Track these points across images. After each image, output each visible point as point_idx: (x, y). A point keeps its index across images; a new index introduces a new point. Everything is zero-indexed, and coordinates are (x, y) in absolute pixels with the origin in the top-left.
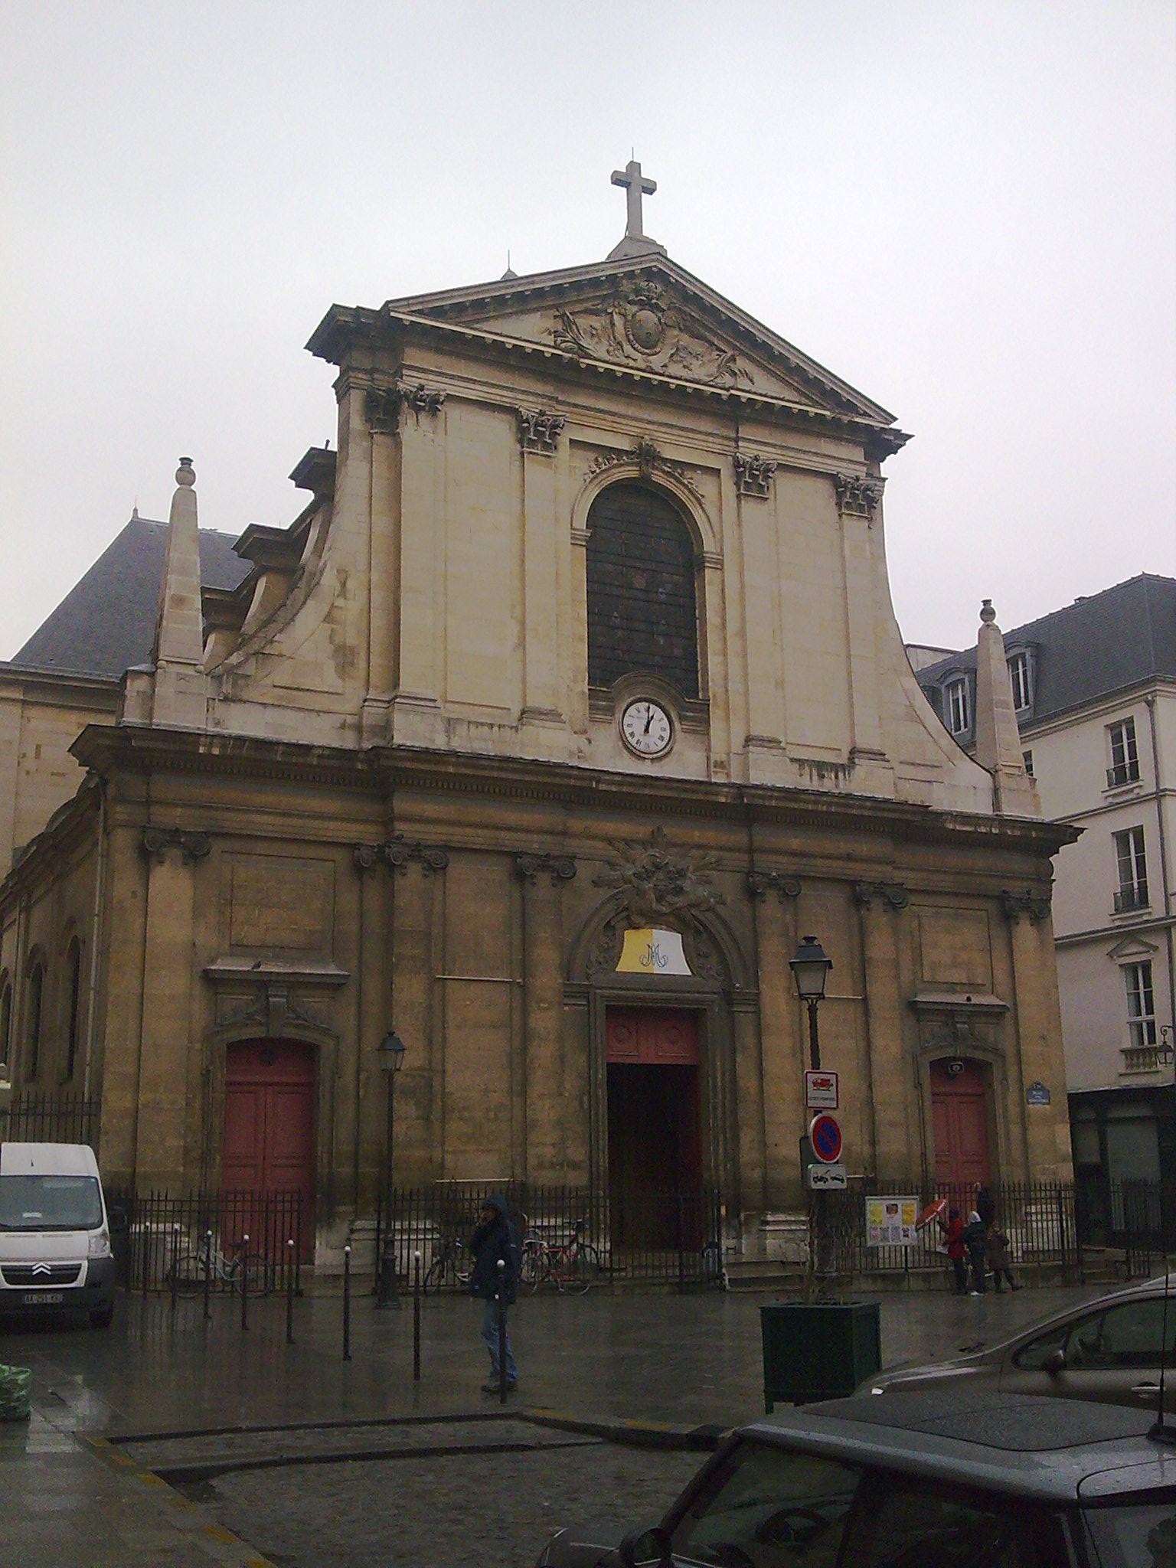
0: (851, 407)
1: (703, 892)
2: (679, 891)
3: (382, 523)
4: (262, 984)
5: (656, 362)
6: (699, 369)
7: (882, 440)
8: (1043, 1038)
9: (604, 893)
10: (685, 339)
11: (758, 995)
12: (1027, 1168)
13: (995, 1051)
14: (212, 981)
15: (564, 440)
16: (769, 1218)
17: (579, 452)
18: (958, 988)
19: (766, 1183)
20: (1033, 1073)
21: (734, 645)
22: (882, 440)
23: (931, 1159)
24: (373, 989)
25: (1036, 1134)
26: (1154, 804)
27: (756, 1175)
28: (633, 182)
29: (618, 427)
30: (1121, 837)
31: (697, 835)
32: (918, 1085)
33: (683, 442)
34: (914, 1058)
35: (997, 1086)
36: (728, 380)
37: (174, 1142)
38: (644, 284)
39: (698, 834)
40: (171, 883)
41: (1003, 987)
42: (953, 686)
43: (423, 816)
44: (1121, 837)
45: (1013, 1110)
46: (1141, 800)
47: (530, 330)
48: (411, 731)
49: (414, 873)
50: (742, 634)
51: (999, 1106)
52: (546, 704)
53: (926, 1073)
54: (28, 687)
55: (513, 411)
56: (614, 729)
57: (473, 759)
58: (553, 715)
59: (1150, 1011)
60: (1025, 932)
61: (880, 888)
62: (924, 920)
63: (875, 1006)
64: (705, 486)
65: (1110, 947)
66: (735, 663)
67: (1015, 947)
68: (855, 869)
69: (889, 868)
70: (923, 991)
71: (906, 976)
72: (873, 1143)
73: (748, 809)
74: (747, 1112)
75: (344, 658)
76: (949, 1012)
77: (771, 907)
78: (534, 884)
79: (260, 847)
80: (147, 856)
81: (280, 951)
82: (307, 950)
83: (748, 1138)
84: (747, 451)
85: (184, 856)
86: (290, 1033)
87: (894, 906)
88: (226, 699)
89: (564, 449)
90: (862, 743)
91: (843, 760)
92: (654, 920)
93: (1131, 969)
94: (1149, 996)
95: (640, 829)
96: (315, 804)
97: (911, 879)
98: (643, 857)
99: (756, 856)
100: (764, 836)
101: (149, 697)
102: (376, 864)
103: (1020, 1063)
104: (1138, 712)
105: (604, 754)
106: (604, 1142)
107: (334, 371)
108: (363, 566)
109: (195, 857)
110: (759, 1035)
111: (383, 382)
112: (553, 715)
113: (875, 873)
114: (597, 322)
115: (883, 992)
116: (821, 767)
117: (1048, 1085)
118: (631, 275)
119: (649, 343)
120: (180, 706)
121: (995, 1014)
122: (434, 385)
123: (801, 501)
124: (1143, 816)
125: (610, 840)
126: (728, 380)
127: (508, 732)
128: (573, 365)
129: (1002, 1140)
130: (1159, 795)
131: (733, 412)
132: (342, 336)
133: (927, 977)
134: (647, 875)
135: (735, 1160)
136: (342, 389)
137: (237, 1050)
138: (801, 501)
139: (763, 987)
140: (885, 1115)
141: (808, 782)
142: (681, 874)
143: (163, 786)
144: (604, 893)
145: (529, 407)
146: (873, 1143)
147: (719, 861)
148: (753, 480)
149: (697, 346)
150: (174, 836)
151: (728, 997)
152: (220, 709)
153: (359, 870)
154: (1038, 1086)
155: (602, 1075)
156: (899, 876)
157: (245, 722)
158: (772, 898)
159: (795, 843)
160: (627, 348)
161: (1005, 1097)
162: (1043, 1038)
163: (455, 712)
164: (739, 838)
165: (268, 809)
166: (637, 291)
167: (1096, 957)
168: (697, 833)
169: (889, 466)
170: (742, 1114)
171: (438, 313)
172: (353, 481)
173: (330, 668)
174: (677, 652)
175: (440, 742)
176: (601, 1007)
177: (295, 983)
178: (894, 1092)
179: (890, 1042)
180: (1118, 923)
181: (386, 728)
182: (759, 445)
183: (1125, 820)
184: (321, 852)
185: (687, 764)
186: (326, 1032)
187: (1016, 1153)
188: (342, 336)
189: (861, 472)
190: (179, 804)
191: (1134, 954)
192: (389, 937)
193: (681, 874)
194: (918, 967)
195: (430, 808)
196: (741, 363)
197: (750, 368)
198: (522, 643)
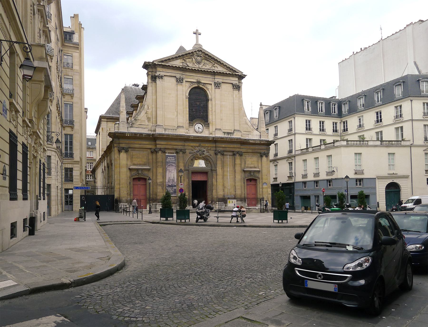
0: (235, 71)
1: (207, 154)
2: (204, 154)
3: (154, 97)
4: (137, 170)
5: (200, 66)
6: (208, 66)
7: (241, 77)
9: (191, 155)
10: (206, 61)
13: (258, 177)
14: (130, 170)
15: (184, 81)
17: (187, 83)
20: (264, 181)
21: (214, 113)
22: (241, 77)
24: (154, 170)
25: (265, 190)
28: (197, 33)
29: (194, 78)
30: (290, 141)
31: (207, 145)
32: (244, 183)
33: (205, 79)
36: (213, 68)
37: (125, 192)
38: (198, 53)
39: (207, 145)
40: (123, 155)
41: (260, 167)
42: (276, 109)
43: (161, 144)
44: (290, 141)
45: (261, 187)
47: (178, 63)
48: (159, 131)
49: (160, 153)
50: (215, 112)
51: (258, 186)
52: (181, 125)
54: (107, 119)
55: (175, 77)
56: (193, 128)
57: (168, 135)
58: (183, 127)
60: (264, 158)
61: (238, 152)
63: (236, 171)
64: (209, 87)
66: (214, 116)
71: (243, 166)
73: (215, 141)
74: (214, 187)
75: (149, 119)
76: (250, 172)
77: (219, 156)
79: (137, 149)
80: (119, 151)
81: (140, 165)
82: (144, 165)
83: (214, 191)
84: (216, 80)
86: (142, 177)
87: (241, 155)
88: (131, 127)
89: (184, 83)
90: (236, 129)
91: (233, 132)
92: (199, 158)
93: (290, 163)
95: (197, 144)
96: (145, 143)
97: (243, 150)
98: (197, 149)
100: (219, 145)
101: (118, 127)
102: (154, 152)
104: (292, 119)
105: (192, 133)
106: (191, 192)
107: (146, 71)
108: (151, 104)
111: (154, 74)
112: (183, 127)
113: (237, 150)
114: (190, 60)
116: (228, 133)
118: (196, 51)
119: (199, 63)
120: (123, 128)
121: (259, 172)
122: (162, 74)
123: (226, 88)
124: (292, 137)
125: (192, 146)
126: (213, 68)
127: (174, 130)
128: (186, 68)
130: (295, 134)
131: (214, 74)
132: (146, 66)
134: (198, 152)
135: (212, 195)
136: (148, 74)
137: (134, 179)
138: (226, 88)
140: (237, 187)
141: (226, 136)
142: (204, 151)
143: (121, 141)
144: (191, 155)
145: (178, 76)
147: (210, 149)
148: (217, 85)
149: (208, 62)
150: (123, 148)
151: (212, 170)
152: (129, 128)
153: (152, 152)
155: (191, 182)
156: (241, 150)
157: (133, 130)
158: (219, 154)
159: (223, 146)
160: (195, 64)
163: (167, 127)
164: (214, 145)
165: (137, 144)
166: (197, 54)
167: (284, 161)
169: (243, 81)
170: (213, 188)
171: (162, 61)
172: (149, 89)
173: (146, 121)
174: (205, 115)
175: (164, 132)
176: (191, 172)
177: (142, 170)
178: (239, 184)
179: (239, 176)
181: (155, 131)
182: (219, 79)
183: (290, 138)
184: (146, 150)
185: (206, 134)
186: (147, 176)
187: (261, 193)
188: (146, 66)
189: (237, 82)
190: (124, 144)
192: (157, 162)
193: (204, 151)
195: (163, 143)
196: (216, 65)
197: (217, 65)
198: (177, 116)
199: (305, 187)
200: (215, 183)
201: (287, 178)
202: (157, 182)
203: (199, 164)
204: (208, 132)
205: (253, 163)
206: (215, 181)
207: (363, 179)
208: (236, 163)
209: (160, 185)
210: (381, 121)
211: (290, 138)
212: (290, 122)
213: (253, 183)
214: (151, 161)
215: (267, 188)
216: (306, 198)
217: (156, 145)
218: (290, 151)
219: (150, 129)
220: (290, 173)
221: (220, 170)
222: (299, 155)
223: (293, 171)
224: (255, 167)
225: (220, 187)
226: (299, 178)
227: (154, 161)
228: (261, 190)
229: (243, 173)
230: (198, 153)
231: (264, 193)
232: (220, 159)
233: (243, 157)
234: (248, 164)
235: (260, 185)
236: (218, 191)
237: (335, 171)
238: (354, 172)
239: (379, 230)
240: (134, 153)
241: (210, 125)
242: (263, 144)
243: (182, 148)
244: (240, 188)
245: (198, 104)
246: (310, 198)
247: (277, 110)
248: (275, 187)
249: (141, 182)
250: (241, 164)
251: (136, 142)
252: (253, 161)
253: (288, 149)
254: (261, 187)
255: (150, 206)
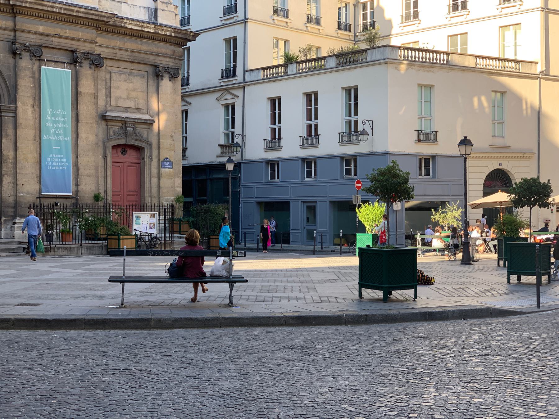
8: (172, 136)
11: (16, 108)
12: (159, 198)
16: (17, 221)
18: (129, 110)
19: (16, 204)
23: (110, 193)
26: (243, 25)
27: (11, 199)
30: (227, 41)
32: (105, 157)
34: (104, 143)
35: (147, 160)
44: (227, 41)
45: (154, 171)
46: (236, 23)
53: (109, 152)
59: (233, 127)
61: (87, 56)
62: (113, 74)
63: (81, 117)
65: (217, 95)
67: (79, 83)
68: (73, 45)
69: (94, 46)
70: (111, 111)
71: (101, 102)
72: (77, 185)
76: (125, 122)
77: (25, 62)
78: (21, 58)
85: (30, 56)
93: (226, 107)
94: (233, 120)
99: (18, 34)
103: (159, 148)
109: (97, 66)
110: (15, 128)
113: (86, 47)
115: (87, 110)
117: (172, 160)
124: (236, 31)
129: (147, 185)
133: (113, 103)
139: (19, 104)
146: (77, 185)
154: (167, 160)
156: (98, 50)
159: (41, 29)
161: (150, 164)
162: (172, 136)
168: (4, 22)
178: (91, 160)
179: (90, 134)
180: (222, 84)
183: (228, 33)
187: (154, 190)
191: (228, 99)
194: (108, 99)
199: (273, 177)
201: (219, 150)
205: (134, 94)
206: (11, 145)
207: (434, 157)
208: (81, 89)
210: (416, 15)
213: (131, 156)
216: (277, 208)
218: (229, 73)
220: (227, 135)
221: (30, 110)
222: (256, 82)
223: (238, 130)
224: (138, 110)
225: (27, 169)
228: (154, 180)
231: (163, 190)
232: (28, 73)
234: (118, 98)
235: (151, 167)
237: (368, 130)
246: (288, 210)
248: (190, 172)
252: (134, 90)
254: (154, 171)
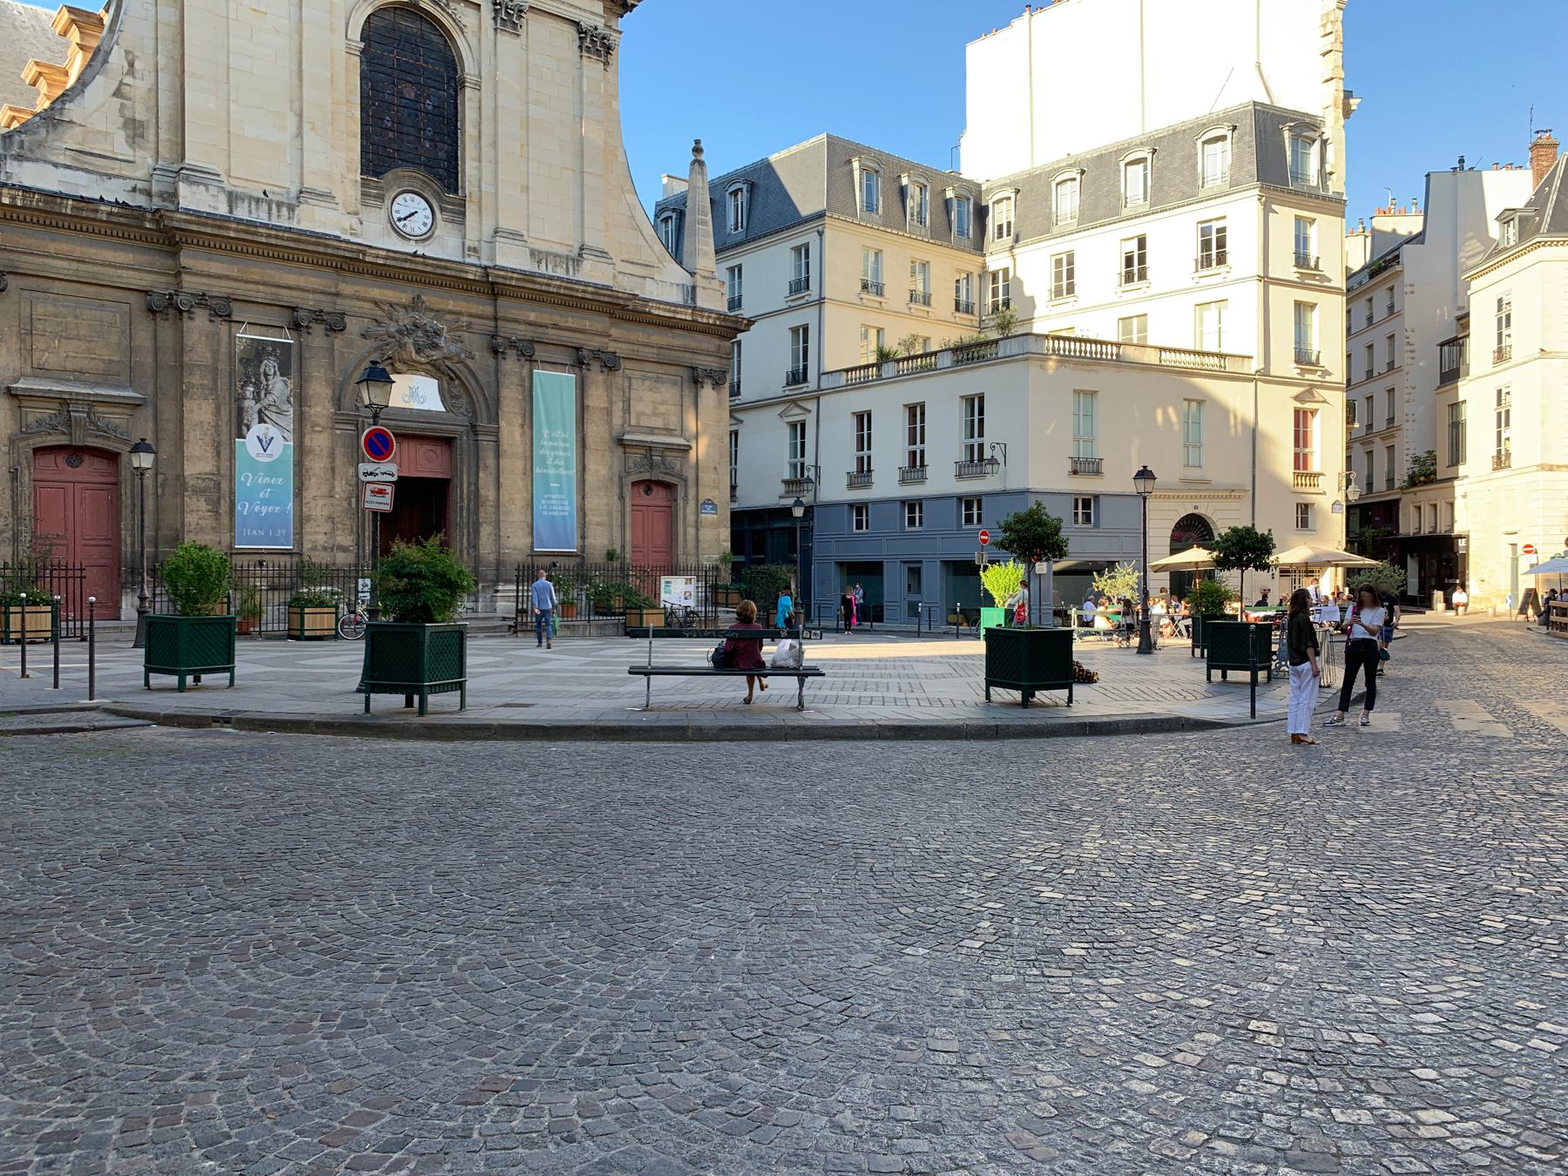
2: (435, 346)
4: (64, 402)
9: (370, 344)
13: (680, 476)
21: (487, 152)
32: (622, 498)
44: (795, 331)
45: (691, 518)
50: (495, 145)
52: (321, 187)
58: (327, 196)
61: (597, 354)
63: (589, 441)
71: (617, 420)
73: (492, 286)
74: (486, 514)
76: (649, 448)
77: (511, 364)
79: (58, 287)
81: (79, 375)
82: (105, 377)
83: (486, 531)
86: (92, 442)
92: (413, 367)
93: (793, 426)
96: (109, 255)
98: (405, 319)
100: (507, 307)
112: (327, 196)
113: (595, 342)
124: (807, 316)
140: (592, 518)
142: (437, 333)
147: (470, 325)
158: (512, 354)
159: (532, 316)
167: (771, 416)
174: (442, 155)
177: (92, 403)
178: (602, 503)
179: (601, 467)
183: (797, 319)
185: (445, 246)
187: (691, 545)
189: (600, 23)
192: (180, 368)
199: (859, 526)
200: (491, 495)
201: (782, 489)
202: (180, 477)
203: (413, 393)
204: (458, 241)
205: (662, 409)
207: (1096, 497)
208: (590, 402)
209: (197, 491)
211: (797, 319)
212: (803, 251)
213: (659, 496)
214: (149, 359)
215: (715, 525)
216: (866, 571)
217: (178, 274)
218: (798, 377)
219: (140, 185)
223: (809, 460)
224: (668, 431)
226: (834, 488)
227: (168, 359)
229: (620, 450)
230: (409, 341)
231: (703, 545)
232: (515, 380)
233: (618, 379)
234: (640, 414)
236: (506, 529)
237: (1000, 459)
238: (1068, 467)
239: (1362, 668)
240: (40, 309)
241: (470, 210)
242: (706, 330)
243: (325, 304)
244: (604, 519)
245: (410, 92)
247: (743, 198)
249: (90, 469)
250: (609, 412)
251: (52, 247)
252: (663, 403)
253: (786, 365)
254: (691, 518)
255: (142, 599)
